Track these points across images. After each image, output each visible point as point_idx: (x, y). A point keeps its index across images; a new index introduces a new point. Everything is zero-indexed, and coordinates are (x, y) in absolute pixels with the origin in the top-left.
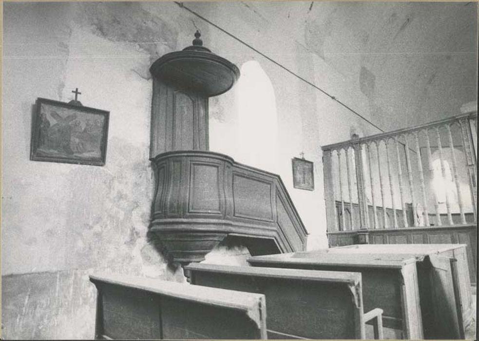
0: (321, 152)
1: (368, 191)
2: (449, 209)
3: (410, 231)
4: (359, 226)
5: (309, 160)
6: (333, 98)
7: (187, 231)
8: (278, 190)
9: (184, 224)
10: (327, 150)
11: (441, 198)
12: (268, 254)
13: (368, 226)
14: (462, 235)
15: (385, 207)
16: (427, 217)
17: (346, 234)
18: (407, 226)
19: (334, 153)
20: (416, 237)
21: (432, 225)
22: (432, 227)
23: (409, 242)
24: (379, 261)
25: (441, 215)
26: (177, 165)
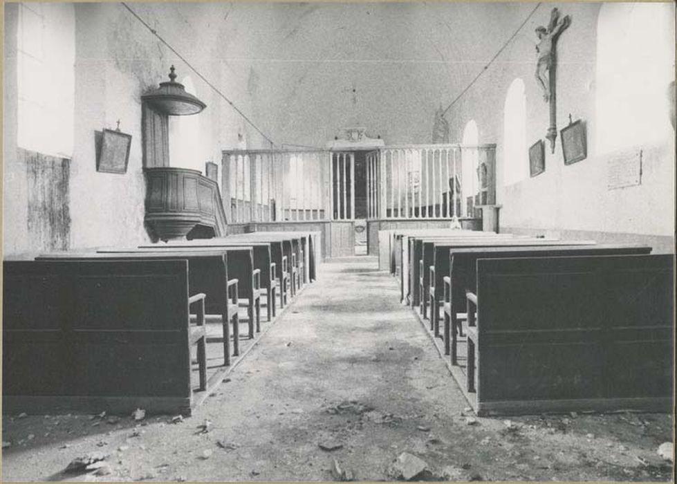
0: (221, 155)
1: (258, 192)
2: (386, 223)
3: (387, 221)
4: (249, 218)
5: (126, 133)
6: (231, 103)
7: (174, 221)
8: (215, 195)
9: (170, 216)
10: (227, 154)
11: (293, 195)
12: (205, 238)
13: (257, 220)
14: (317, 227)
15: (238, 198)
16: (284, 211)
17: (238, 225)
18: (271, 221)
19: (233, 157)
20: (289, 228)
21: (287, 219)
22: (287, 221)
23: (284, 230)
24: (643, 154)
25: (292, 210)
26: (174, 177)
